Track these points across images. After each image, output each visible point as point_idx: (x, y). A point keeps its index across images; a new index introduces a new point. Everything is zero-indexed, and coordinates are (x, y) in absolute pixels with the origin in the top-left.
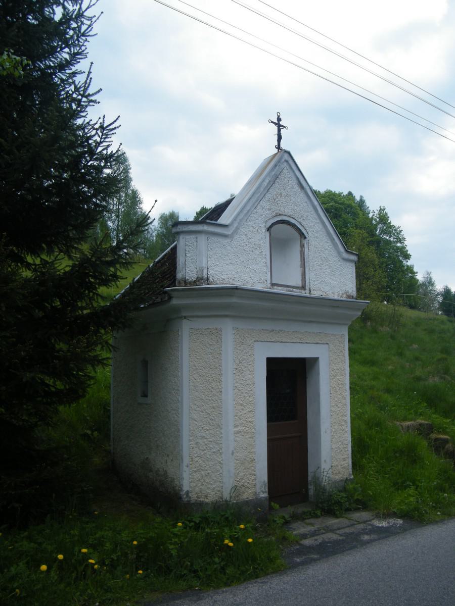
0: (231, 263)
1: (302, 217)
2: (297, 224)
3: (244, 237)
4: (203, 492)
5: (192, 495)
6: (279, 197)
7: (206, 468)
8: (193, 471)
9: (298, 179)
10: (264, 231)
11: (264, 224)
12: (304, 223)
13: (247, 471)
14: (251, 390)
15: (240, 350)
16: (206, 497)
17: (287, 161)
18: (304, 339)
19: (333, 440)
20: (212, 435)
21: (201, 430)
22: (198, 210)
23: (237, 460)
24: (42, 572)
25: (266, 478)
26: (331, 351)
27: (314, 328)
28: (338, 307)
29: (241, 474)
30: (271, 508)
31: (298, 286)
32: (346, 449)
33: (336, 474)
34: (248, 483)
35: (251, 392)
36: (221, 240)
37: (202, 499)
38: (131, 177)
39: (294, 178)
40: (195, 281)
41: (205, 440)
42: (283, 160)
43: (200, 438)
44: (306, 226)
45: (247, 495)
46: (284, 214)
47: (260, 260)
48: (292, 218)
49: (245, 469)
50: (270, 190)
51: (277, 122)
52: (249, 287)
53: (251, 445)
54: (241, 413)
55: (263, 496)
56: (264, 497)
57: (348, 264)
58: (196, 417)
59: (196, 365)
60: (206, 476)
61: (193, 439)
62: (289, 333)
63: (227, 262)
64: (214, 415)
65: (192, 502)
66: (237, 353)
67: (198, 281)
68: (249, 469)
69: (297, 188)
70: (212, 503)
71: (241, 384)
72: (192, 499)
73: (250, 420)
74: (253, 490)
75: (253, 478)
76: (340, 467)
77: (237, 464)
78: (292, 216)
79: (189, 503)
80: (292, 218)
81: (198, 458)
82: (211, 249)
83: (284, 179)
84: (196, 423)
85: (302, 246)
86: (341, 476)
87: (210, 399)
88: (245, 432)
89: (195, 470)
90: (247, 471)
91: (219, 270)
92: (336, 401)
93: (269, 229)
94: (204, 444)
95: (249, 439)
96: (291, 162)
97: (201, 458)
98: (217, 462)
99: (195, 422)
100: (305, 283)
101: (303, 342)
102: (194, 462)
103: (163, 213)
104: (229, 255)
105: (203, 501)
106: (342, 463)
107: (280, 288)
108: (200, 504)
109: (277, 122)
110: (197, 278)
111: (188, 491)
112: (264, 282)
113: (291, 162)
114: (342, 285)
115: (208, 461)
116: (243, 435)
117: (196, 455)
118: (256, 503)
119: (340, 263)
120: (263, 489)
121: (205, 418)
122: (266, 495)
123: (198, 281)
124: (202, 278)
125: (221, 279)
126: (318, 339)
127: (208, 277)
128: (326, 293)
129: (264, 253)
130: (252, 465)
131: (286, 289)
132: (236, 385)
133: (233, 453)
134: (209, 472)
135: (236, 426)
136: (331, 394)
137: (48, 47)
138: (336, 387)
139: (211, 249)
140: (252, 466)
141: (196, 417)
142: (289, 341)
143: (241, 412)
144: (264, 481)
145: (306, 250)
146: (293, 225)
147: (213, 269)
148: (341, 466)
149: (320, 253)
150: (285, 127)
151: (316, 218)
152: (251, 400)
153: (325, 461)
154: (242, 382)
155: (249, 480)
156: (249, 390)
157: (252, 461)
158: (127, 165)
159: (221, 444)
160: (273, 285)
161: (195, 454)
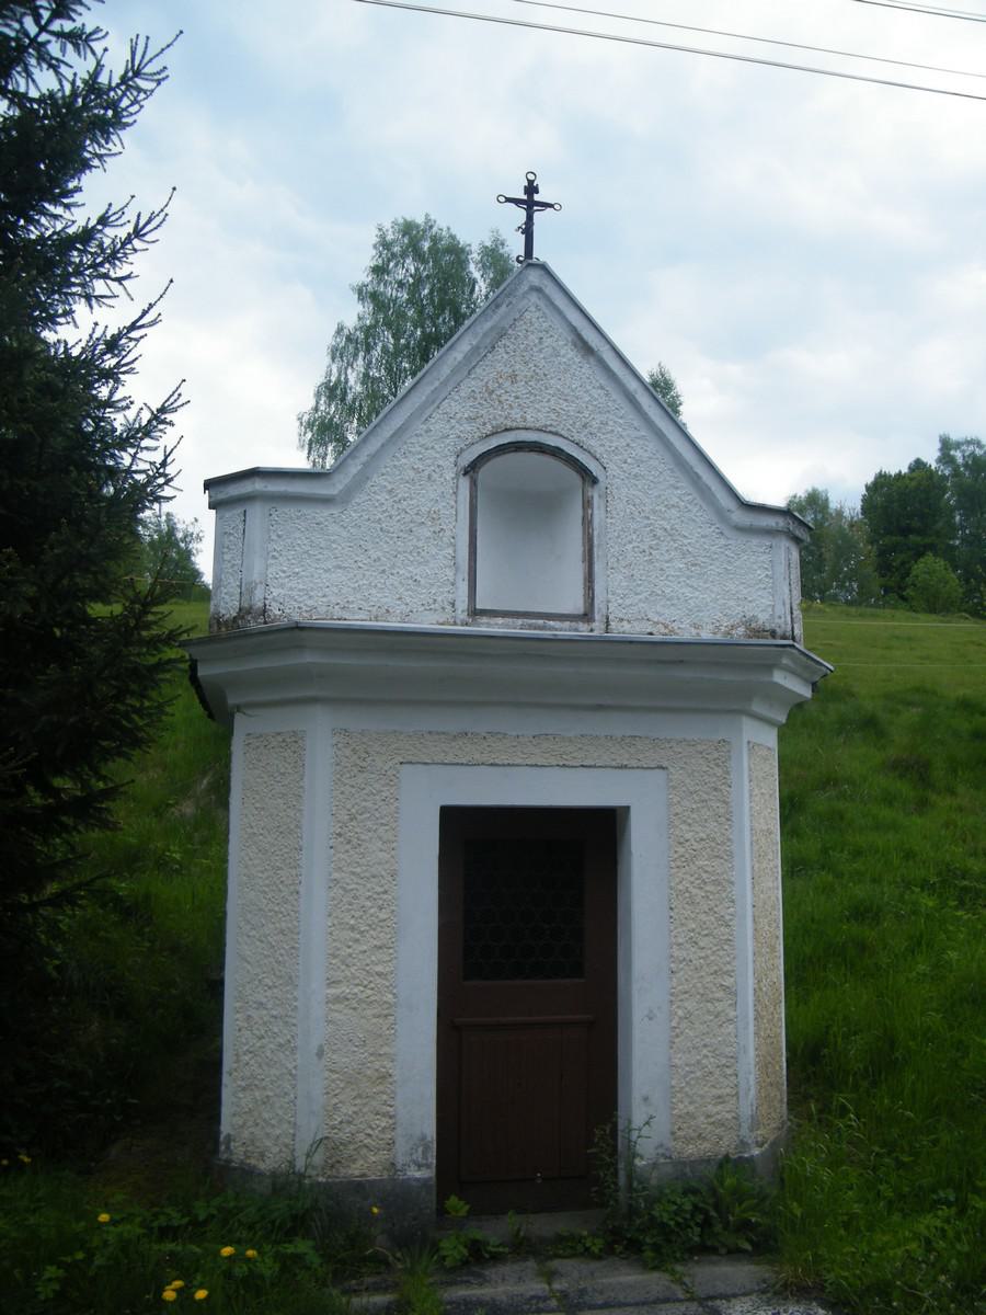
0: (340, 567)
1: (585, 426)
2: (565, 448)
3: (383, 497)
4: (258, 1144)
5: (236, 1148)
6: (507, 384)
7: (264, 1084)
8: (239, 1086)
9: (574, 330)
10: (449, 475)
11: (452, 459)
12: (592, 443)
13: (365, 1105)
14: (386, 892)
15: (353, 786)
16: (262, 1156)
17: (538, 290)
18: (575, 755)
19: (676, 1040)
20: (278, 1002)
21: (257, 987)
22: (870, 479)
23: (332, 1071)
24: (201, 1287)
25: (430, 1129)
26: (674, 788)
27: (619, 725)
28: (682, 662)
29: (347, 1109)
30: (441, 1211)
31: (576, 612)
32: (729, 1071)
33: (688, 1140)
34: (369, 1135)
35: (385, 896)
36: (308, 511)
37: (253, 1162)
38: (684, 421)
39: (561, 330)
40: (235, 618)
41: (265, 1012)
42: (525, 287)
43: (255, 1005)
44: (599, 451)
45: (364, 1166)
46: (522, 425)
47: (434, 551)
48: (550, 432)
49: (359, 1096)
50: (478, 370)
51: (525, 197)
52: (393, 624)
53: (380, 1036)
54: (350, 950)
55: (418, 1175)
56: (417, 1180)
57: (755, 541)
58: (249, 953)
59: (254, 824)
60: (264, 1103)
61: (241, 1008)
62: (521, 739)
63: (329, 565)
64: (282, 951)
65: (233, 1164)
66: (342, 793)
67: (243, 618)
68: (373, 1098)
69: (570, 354)
70: (274, 1174)
71: (353, 873)
72: (234, 1157)
73: (379, 968)
74: (383, 1156)
75: (383, 1124)
76: (702, 1119)
77: (333, 1081)
78: (549, 429)
79: (226, 1168)
80: (550, 432)
81: (250, 1055)
82: (279, 536)
83: (526, 337)
84: (249, 967)
85: (587, 504)
86: (706, 1145)
87: (276, 909)
88: (360, 1001)
89: (243, 1084)
90: (365, 1105)
91: (301, 586)
92: (693, 930)
93: (472, 469)
94: (261, 1022)
95: (375, 1020)
96: (550, 289)
97: (256, 1055)
98: (285, 1071)
99: (246, 964)
100: (592, 604)
101: (570, 763)
102: (241, 1064)
103: (792, 494)
104: (334, 546)
105: (254, 1166)
106: (712, 1109)
107: (500, 621)
108: (248, 1172)
109: (525, 197)
110: (240, 609)
111: (229, 1135)
112: (443, 608)
113: (550, 289)
114: (732, 603)
115: (267, 1064)
116: (355, 1009)
117: (245, 1048)
118: (395, 1195)
119: (723, 541)
120: (418, 1155)
121: (266, 956)
122: (428, 1173)
123: (243, 618)
124: (251, 608)
125: (304, 608)
126: (627, 756)
127: (265, 605)
128: (666, 627)
129: (448, 533)
130: (381, 1088)
131: (520, 622)
132: (336, 875)
133: (320, 1054)
134: (271, 1094)
135: (332, 983)
136: (671, 909)
137: (94, 148)
138: (694, 891)
139: (279, 536)
140: (383, 1093)
141: (249, 953)
142: (519, 761)
143: (349, 947)
144: (423, 1138)
145: (598, 515)
146: (556, 452)
147: (282, 586)
148: (708, 1116)
149: (648, 518)
150: (551, 206)
151: (636, 424)
152: (383, 915)
153: (646, 1099)
154: (358, 870)
155: (373, 1129)
156: (380, 890)
157: (384, 1077)
158: (673, 397)
159: (294, 1025)
160: (475, 613)
161: (245, 1045)
